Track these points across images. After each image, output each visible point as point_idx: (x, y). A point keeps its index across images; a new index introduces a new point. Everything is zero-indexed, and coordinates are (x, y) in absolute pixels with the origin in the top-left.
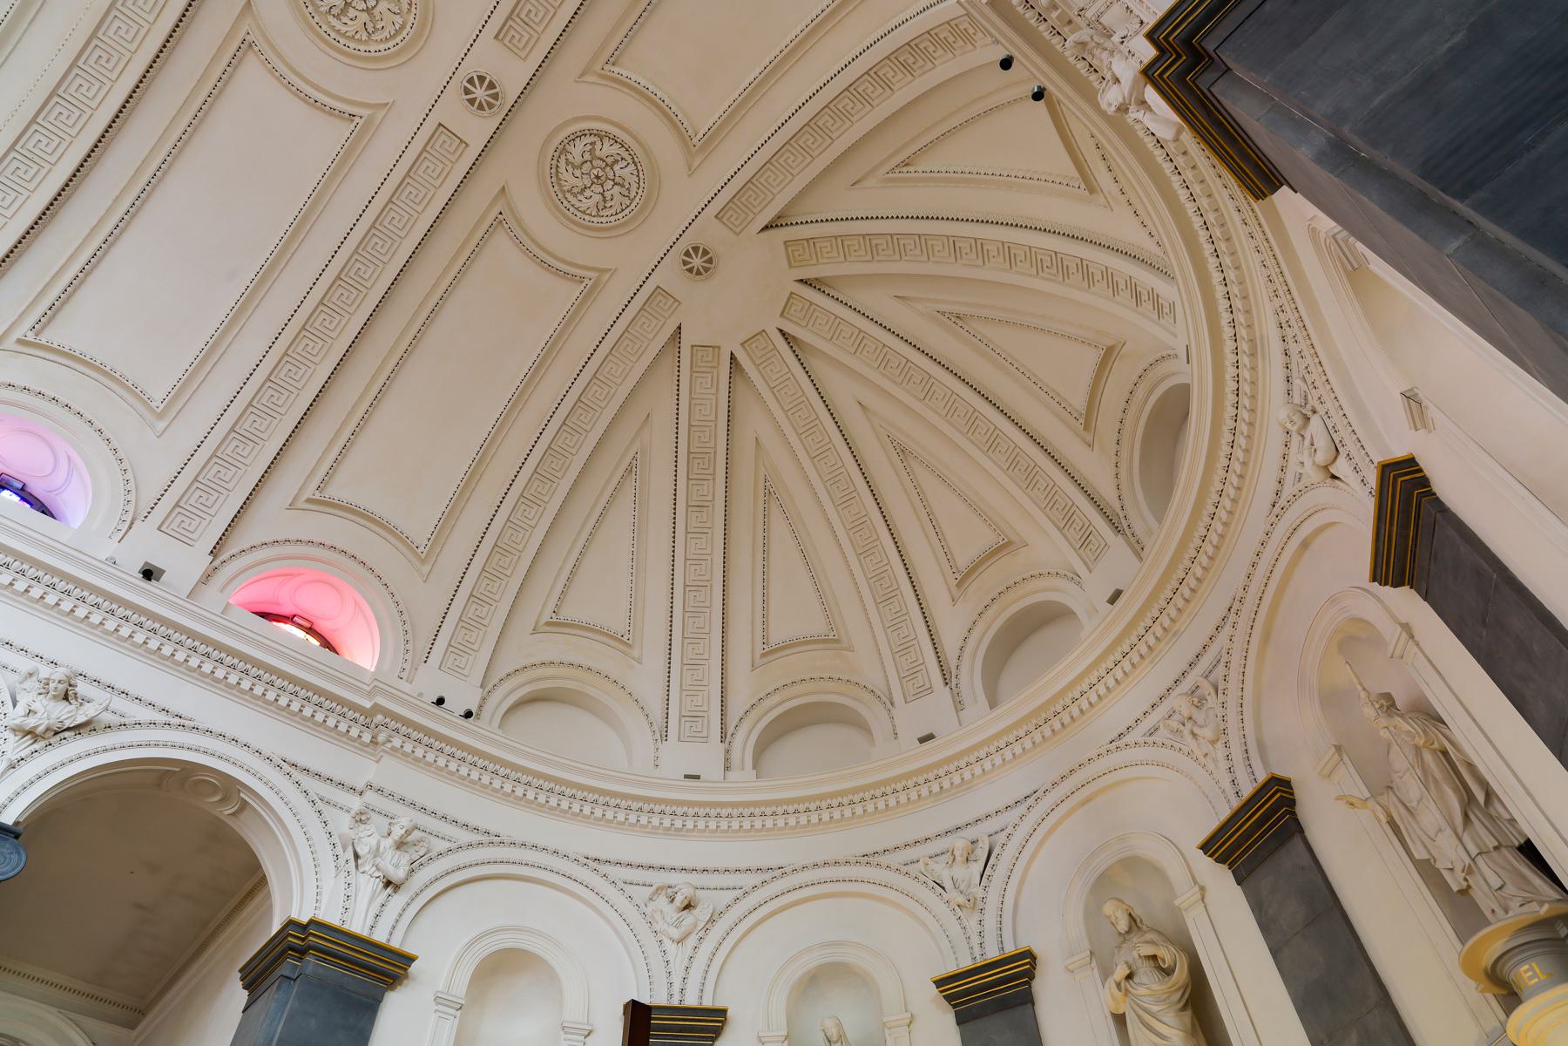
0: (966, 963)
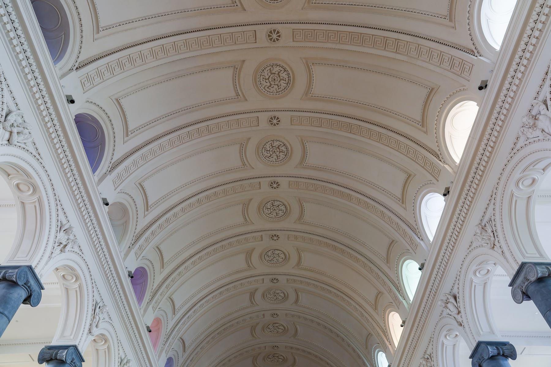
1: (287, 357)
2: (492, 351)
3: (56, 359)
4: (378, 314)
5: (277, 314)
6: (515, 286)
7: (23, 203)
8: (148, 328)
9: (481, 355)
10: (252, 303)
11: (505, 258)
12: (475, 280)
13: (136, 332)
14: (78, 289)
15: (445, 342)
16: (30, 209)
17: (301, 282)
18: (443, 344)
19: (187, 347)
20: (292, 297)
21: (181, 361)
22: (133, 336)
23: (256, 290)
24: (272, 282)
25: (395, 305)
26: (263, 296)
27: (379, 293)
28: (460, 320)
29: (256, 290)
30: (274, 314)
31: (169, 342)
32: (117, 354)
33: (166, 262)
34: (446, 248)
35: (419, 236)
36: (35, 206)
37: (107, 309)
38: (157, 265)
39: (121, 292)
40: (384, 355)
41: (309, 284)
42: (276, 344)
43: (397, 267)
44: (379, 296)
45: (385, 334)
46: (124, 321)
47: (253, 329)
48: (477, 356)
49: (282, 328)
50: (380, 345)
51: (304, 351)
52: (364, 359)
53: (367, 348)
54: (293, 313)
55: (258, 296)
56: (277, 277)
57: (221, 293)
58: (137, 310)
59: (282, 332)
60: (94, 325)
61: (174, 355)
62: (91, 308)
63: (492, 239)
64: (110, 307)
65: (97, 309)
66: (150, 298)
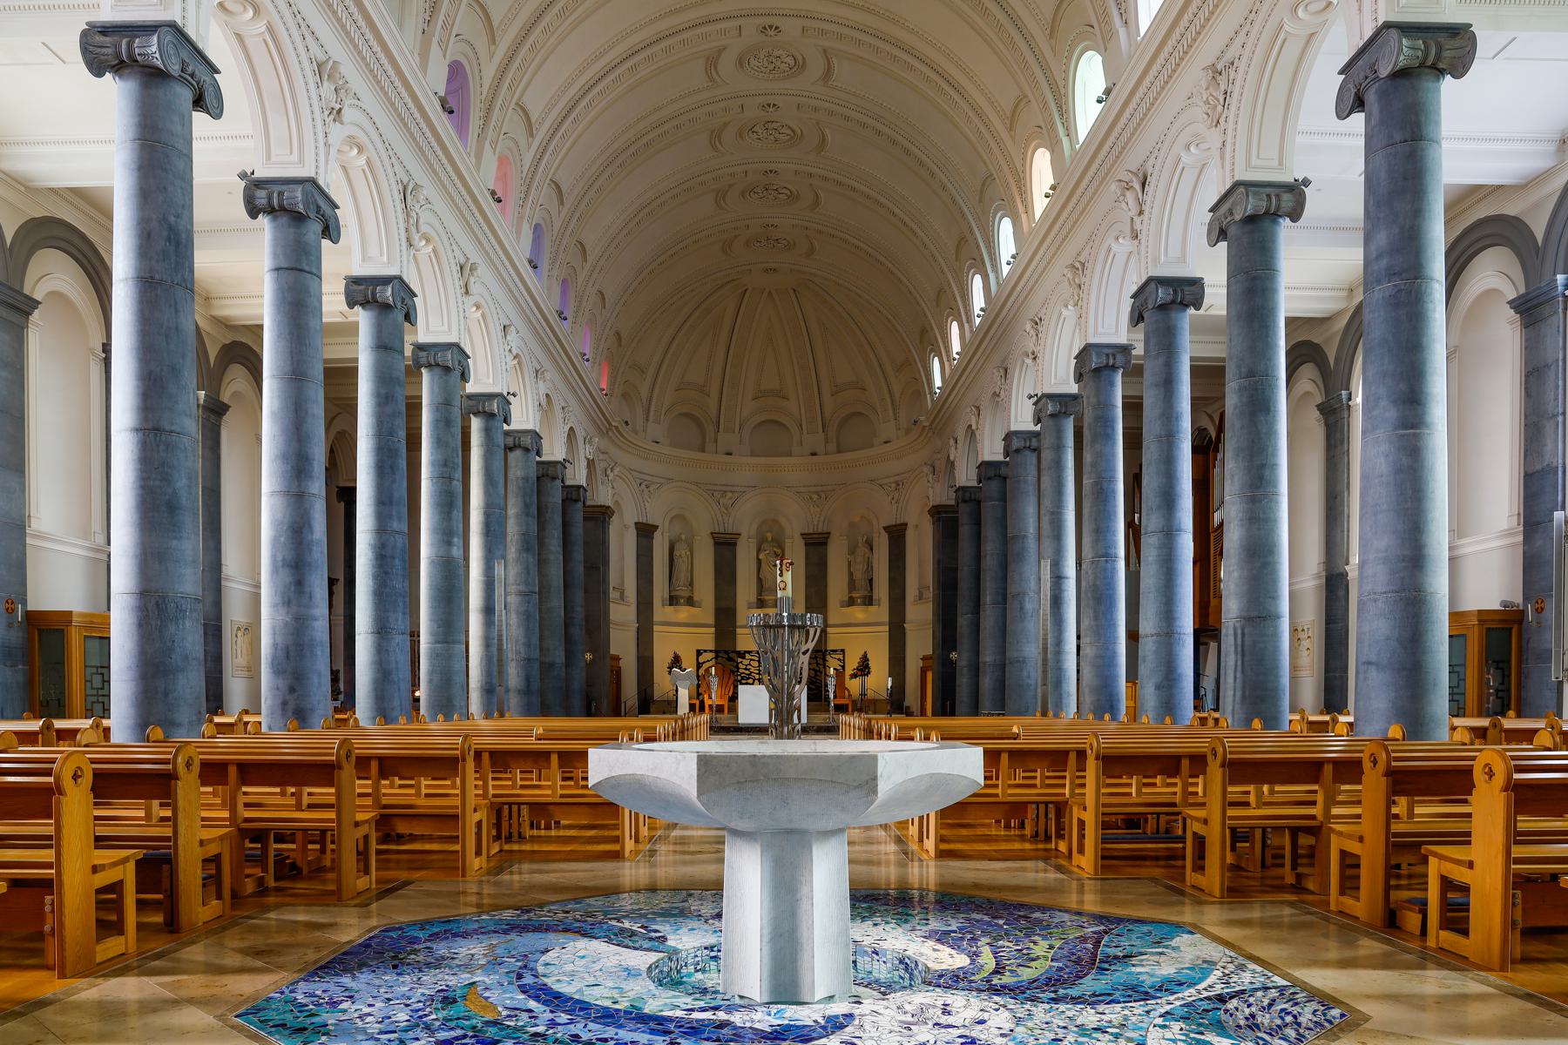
0: (811, 531)
1: (804, 58)
2: (1162, 294)
3: (571, 499)
4: (1013, 139)
5: (774, 105)
6: (1217, 214)
7: (239, 37)
8: (493, 193)
9: (1146, 300)
10: (711, 79)
11: (1222, 158)
12: (1185, 159)
13: (473, 207)
14: (366, 168)
15: (1115, 247)
16: (256, 46)
17: (841, 37)
18: (1109, 250)
19: (565, 196)
20: (816, 67)
21: (558, 223)
22: (457, 198)
23: (721, 50)
24: (763, 35)
25: (1046, 134)
26: (741, 62)
27: (1021, 100)
28: (1138, 226)
29: (721, 50)
30: (769, 105)
31: (531, 198)
32: (452, 260)
33: (501, 23)
34: (1196, 11)
35: (1122, 11)
36: (265, 41)
37: (425, 192)
38: (481, 43)
39: (423, 125)
40: (1048, 154)
41: (860, 42)
42: (773, 167)
43: (1069, 58)
44: (1020, 108)
45: (1061, 107)
46: (459, 209)
47: (716, 136)
48: (1142, 298)
49: (789, 132)
50: (1006, 203)
51: (840, 184)
52: (973, 223)
53: (981, 201)
54: (814, 103)
55: (727, 64)
56: (776, 21)
57: (632, 69)
58: (463, 158)
59: (788, 141)
60: (413, 229)
61: (509, 149)
62: (398, 197)
63: (1220, 108)
64: (429, 190)
65: (409, 197)
66: (482, 122)
